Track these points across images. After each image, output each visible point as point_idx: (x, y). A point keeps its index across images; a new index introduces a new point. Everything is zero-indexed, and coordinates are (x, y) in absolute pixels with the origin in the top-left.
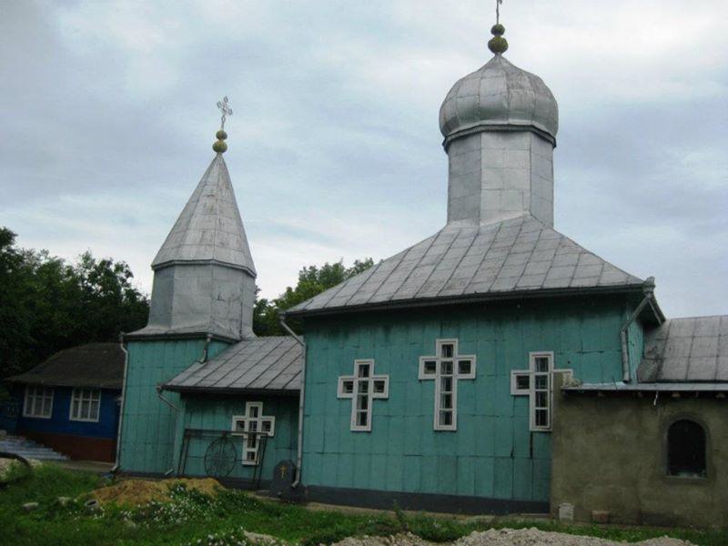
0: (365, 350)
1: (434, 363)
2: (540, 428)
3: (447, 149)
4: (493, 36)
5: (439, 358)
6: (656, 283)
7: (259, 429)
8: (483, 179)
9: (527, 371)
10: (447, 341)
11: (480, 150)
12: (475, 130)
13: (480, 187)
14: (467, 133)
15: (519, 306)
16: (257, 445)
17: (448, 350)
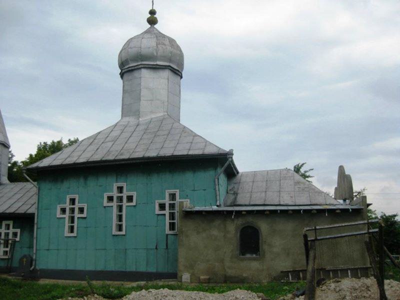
2: (171, 232)
7: (11, 237)
8: (141, 95)
10: (120, 184)
11: (141, 78)
14: (133, 68)
16: (9, 246)
17: (120, 189)
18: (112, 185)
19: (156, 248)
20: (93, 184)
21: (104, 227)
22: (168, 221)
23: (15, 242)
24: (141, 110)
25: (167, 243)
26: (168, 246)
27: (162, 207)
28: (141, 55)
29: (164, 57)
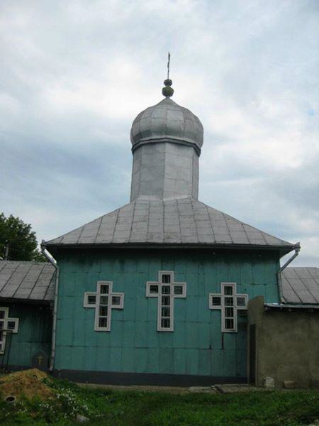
0: (107, 275)
1: (157, 286)
2: (229, 330)
3: (133, 153)
4: (165, 86)
5: (160, 284)
6: (301, 246)
8: (166, 172)
9: (94, 293)
10: (166, 272)
11: (165, 153)
12: (161, 141)
13: (163, 176)
14: (156, 141)
15: (214, 253)
17: (166, 278)
18: (156, 273)
19: (210, 348)
20: (134, 271)
21: (147, 322)
22: (224, 317)
23: (10, 335)
24: (165, 189)
25: (223, 340)
26: (224, 346)
27: (217, 301)
28: (166, 128)
29: (190, 133)
